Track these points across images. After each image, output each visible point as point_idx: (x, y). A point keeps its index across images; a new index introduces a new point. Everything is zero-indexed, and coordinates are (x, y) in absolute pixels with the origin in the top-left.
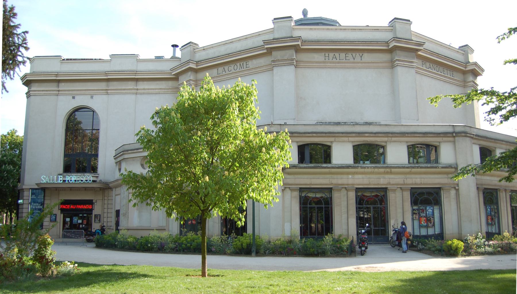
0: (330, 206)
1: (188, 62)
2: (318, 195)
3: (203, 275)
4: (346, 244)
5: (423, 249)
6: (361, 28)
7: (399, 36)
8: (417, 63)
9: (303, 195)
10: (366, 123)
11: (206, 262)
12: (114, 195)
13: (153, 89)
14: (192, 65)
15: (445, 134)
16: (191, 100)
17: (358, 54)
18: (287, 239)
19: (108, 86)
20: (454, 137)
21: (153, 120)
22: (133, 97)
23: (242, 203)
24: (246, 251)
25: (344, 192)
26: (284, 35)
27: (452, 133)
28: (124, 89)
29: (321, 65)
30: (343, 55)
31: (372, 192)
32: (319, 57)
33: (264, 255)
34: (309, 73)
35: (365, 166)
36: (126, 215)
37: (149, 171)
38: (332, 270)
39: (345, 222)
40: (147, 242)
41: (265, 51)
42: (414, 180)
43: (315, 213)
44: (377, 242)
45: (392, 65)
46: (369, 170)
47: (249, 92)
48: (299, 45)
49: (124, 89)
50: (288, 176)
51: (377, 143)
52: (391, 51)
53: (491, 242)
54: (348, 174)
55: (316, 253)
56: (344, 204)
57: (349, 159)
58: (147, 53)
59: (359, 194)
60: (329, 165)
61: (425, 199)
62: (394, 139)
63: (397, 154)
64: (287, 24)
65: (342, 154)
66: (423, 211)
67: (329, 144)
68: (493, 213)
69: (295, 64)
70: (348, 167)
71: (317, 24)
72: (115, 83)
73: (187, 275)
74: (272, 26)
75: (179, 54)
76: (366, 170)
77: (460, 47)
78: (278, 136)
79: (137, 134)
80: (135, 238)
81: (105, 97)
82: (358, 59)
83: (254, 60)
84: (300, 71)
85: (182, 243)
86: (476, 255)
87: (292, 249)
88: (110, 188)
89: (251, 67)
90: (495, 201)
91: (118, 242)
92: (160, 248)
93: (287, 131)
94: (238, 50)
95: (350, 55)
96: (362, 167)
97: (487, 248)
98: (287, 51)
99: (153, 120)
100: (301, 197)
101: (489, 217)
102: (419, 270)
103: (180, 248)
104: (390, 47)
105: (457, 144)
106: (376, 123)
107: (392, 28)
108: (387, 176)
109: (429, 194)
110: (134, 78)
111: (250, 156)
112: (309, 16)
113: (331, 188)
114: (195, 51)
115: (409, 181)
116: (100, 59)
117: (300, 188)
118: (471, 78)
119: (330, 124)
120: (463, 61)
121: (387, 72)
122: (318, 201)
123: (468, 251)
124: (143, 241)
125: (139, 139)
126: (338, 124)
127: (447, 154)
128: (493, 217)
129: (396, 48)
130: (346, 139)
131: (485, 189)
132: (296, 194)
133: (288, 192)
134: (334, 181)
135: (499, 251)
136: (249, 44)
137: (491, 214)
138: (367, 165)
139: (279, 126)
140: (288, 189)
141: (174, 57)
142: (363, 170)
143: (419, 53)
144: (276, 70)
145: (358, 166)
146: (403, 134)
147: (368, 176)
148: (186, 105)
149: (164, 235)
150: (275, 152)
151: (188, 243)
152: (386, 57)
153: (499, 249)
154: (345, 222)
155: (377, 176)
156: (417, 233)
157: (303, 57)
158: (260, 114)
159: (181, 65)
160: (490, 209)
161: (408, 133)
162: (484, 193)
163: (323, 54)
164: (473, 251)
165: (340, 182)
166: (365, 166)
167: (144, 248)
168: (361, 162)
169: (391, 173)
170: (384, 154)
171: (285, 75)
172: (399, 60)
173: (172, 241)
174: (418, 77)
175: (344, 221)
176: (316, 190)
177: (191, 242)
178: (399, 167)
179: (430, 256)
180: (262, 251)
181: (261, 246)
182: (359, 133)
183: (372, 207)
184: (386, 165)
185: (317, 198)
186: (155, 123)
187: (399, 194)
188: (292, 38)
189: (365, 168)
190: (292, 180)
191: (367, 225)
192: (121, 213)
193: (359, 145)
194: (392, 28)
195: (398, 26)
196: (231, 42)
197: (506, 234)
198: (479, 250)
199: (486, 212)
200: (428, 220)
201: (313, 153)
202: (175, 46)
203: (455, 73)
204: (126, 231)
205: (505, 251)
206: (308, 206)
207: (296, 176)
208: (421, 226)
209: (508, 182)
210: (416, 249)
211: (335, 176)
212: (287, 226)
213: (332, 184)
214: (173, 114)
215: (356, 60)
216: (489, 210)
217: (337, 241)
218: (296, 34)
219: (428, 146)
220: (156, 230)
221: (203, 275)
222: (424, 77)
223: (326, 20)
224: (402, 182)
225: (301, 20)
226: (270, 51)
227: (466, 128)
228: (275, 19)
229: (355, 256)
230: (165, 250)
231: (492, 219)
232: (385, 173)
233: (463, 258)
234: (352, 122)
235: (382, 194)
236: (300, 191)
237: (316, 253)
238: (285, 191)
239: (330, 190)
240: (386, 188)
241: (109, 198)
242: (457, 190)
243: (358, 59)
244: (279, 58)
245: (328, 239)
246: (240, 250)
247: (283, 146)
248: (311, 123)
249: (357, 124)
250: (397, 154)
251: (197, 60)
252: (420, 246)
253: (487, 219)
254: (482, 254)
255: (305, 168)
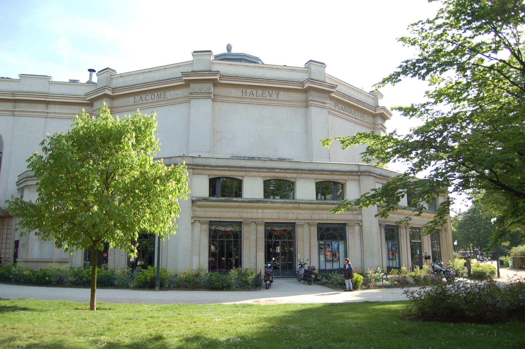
0: (239, 240)
1: (104, 88)
2: (229, 229)
3: (92, 308)
4: (251, 278)
5: (327, 282)
6: (278, 67)
7: (313, 78)
8: (330, 104)
9: (213, 228)
10: (280, 159)
11: (96, 295)
12: (14, 225)
13: (65, 114)
14: (109, 91)
15: (351, 173)
16: (85, 128)
17: (274, 92)
18: (194, 272)
19: (15, 107)
20: (359, 175)
21: (43, 146)
22: (43, 120)
23: (134, 235)
24: (149, 285)
25: (253, 226)
26: (203, 68)
27: (358, 172)
28: (33, 112)
29: (239, 100)
30: (260, 92)
31: (281, 226)
32: (236, 92)
33: (169, 288)
34: (226, 108)
35: (274, 200)
36: (26, 246)
37: (38, 199)
38: (227, 303)
39: (253, 256)
40: (45, 275)
41: (183, 83)
42: (321, 215)
43: (225, 248)
44: (285, 276)
45: (306, 105)
46: (279, 205)
47: (148, 124)
48: (217, 79)
49: (33, 112)
50: (198, 209)
51: (287, 179)
52: (306, 91)
53: (389, 276)
54: (258, 208)
55: (221, 286)
56: (253, 238)
57: (260, 195)
58: (61, 74)
59: (268, 228)
60: (240, 199)
61: (331, 234)
62: (303, 175)
63: (305, 190)
64: (207, 57)
65: (253, 188)
66: (329, 245)
67: (240, 178)
68: (394, 249)
69: (212, 97)
70: (258, 201)
71: (240, 60)
72: (23, 105)
73: (76, 309)
74: (191, 58)
75: (95, 79)
76: (275, 205)
77: (371, 92)
78: (175, 168)
79: (29, 160)
80: (32, 271)
81: (11, 119)
82: (274, 97)
83: (172, 91)
84: (218, 105)
85: (83, 277)
86: (374, 288)
87: (197, 283)
88: (10, 217)
89: (169, 97)
90: (236, 229)
91: (13, 275)
92: (60, 282)
93: (184, 164)
94: (156, 79)
95: (266, 92)
96: (271, 202)
97: (384, 281)
98: (205, 84)
99: (43, 146)
100: (210, 230)
101: (391, 252)
102: (309, 302)
103: (80, 282)
104: (305, 87)
105: (361, 182)
106: (289, 159)
107: (307, 69)
108: (296, 211)
109: (335, 229)
110: (45, 101)
111: (145, 188)
112: (234, 51)
113: (241, 222)
114: (112, 77)
115: (316, 217)
116: (7, 78)
117: (210, 221)
118: (379, 121)
119: (244, 158)
120: (373, 105)
121: (301, 111)
122: (227, 234)
123: (367, 285)
124: (41, 274)
125: (30, 165)
126: (252, 159)
127: (352, 192)
128: (394, 252)
129: (310, 89)
130: (257, 174)
131: (387, 225)
132: (206, 227)
133: (198, 226)
134: (244, 215)
135: (395, 284)
136: (168, 74)
137: (392, 249)
138: (277, 201)
139: (191, 159)
140: (197, 222)
141: (90, 82)
142: (272, 205)
143: (332, 95)
144: (193, 102)
145: (268, 201)
146: (312, 171)
147: (277, 211)
148: (81, 132)
149: (65, 267)
150: (172, 184)
151: (89, 276)
152: (301, 97)
153: (396, 282)
154: (253, 256)
155: (286, 211)
156: (323, 267)
157: (221, 91)
158: (160, 146)
159: (96, 91)
160: (392, 245)
161: (316, 171)
162: (385, 230)
163: (241, 89)
164: (371, 285)
165: (250, 216)
166: (274, 200)
167: (41, 281)
168: (272, 197)
169: (299, 208)
170: (293, 190)
171: (202, 108)
172: (312, 101)
173: (73, 274)
174: (331, 117)
175: (253, 254)
176: (225, 223)
177: (94, 275)
178: (307, 203)
179: (329, 289)
180: (167, 285)
181: (165, 279)
182: (270, 169)
183: (280, 241)
184: (295, 201)
185: (227, 232)
186: (45, 149)
187: (306, 229)
188: (211, 72)
189: (274, 203)
190: (201, 212)
191: (274, 259)
192: (20, 243)
193: (320, 182)
194: (307, 69)
195: (313, 67)
196: (150, 71)
197: (404, 268)
198: (378, 284)
199: (388, 249)
200: (334, 255)
201: (225, 187)
202: (92, 71)
203: (365, 116)
204: (22, 263)
205: (401, 284)
206: (218, 239)
207: (206, 209)
208: (326, 261)
209: (384, 218)
210: (320, 282)
211: (245, 210)
212: (195, 259)
213: (242, 218)
214: (64, 141)
215: (272, 98)
216: (390, 245)
217: (244, 275)
218: (215, 68)
219: (335, 183)
220: (56, 262)
221: (92, 308)
222: (336, 118)
223: (249, 56)
224: (310, 218)
225: (224, 55)
226: (188, 83)
227: (370, 167)
228: (195, 52)
229: (260, 290)
230: (64, 284)
231: (393, 254)
232: (293, 208)
233: (362, 291)
234: (266, 158)
235: (291, 229)
236: (210, 224)
237: (221, 286)
238: (194, 224)
239: (240, 224)
240: (295, 223)
241: (9, 227)
242: (361, 226)
243: (274, 97)
244: (197, 91)
245: (233, 272)
246: (143, 283)
247: (180, 178)
248: (226, 156)
249: (271, 160)
250: (305, 190)
251: (113, 86)
252: (324, 280)
253: (389, 254)
254: (380, 287)
255: (215, 201)
